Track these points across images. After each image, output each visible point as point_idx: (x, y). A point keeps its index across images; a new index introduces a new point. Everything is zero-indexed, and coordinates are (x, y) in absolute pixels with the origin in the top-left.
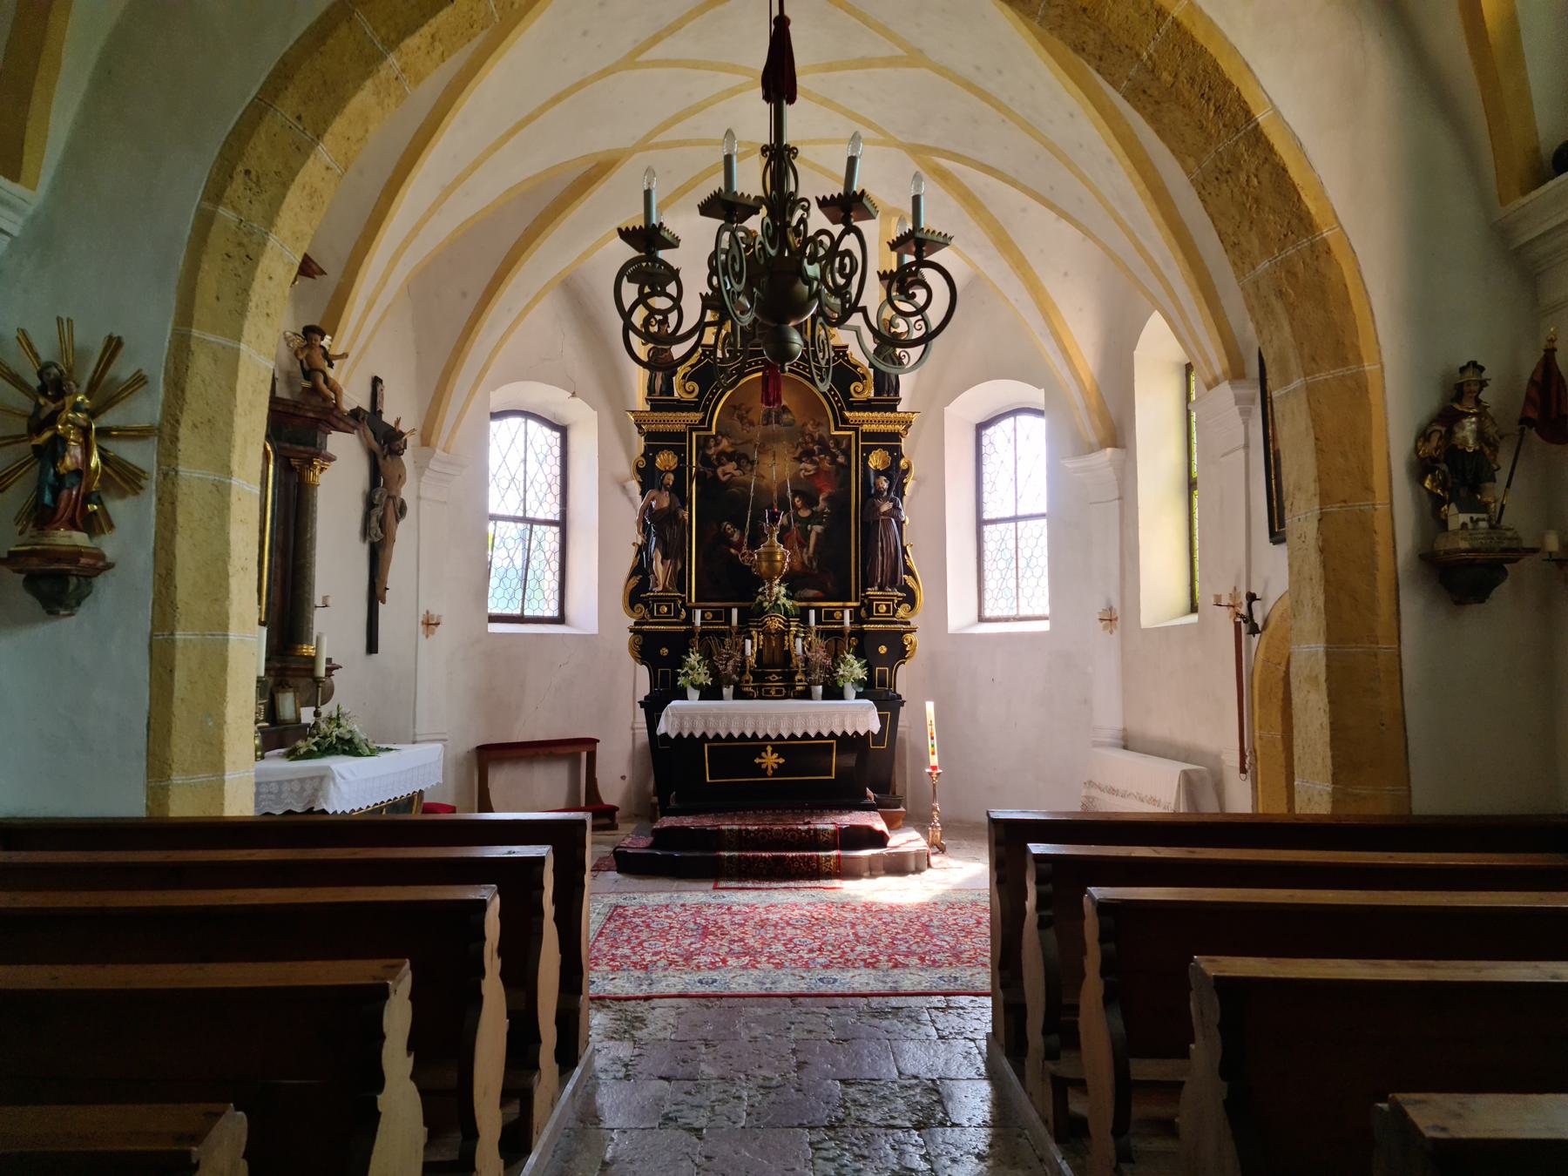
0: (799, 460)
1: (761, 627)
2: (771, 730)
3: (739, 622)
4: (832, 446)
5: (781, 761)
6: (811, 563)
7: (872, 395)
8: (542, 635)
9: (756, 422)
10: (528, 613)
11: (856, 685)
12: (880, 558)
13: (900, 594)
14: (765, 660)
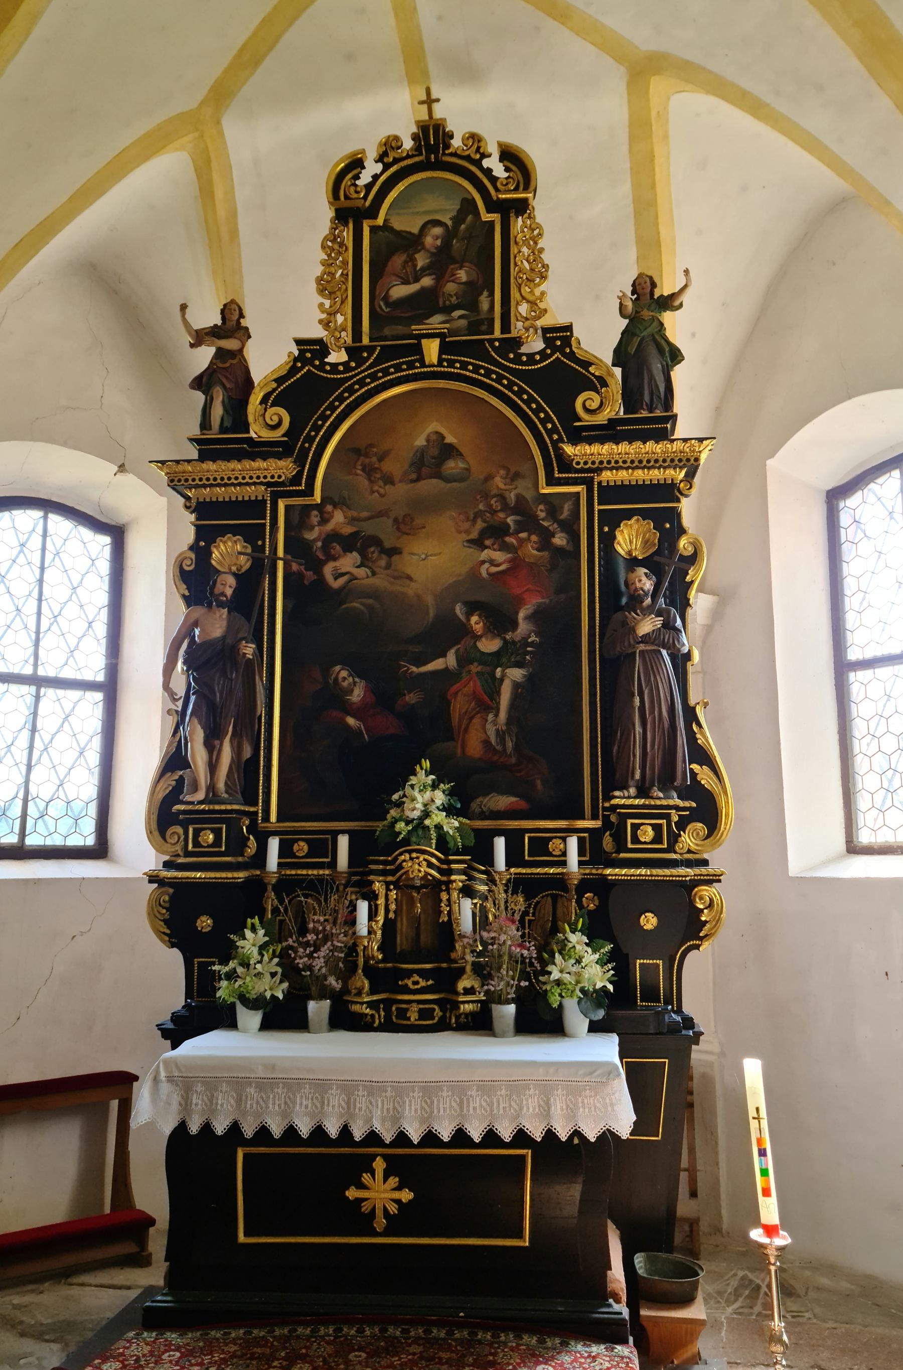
0: (479, 543)
1: (393, 873)
2: (383, 1120)
3: (352, 862)
4: (542, 515)
5: (406, 1196)
7: (622, 413)
8: (37, 882)
10: (31, 841)
11: (587, 1004)
12: (638, 729)
13: (681, 803)
14: (402, 941)
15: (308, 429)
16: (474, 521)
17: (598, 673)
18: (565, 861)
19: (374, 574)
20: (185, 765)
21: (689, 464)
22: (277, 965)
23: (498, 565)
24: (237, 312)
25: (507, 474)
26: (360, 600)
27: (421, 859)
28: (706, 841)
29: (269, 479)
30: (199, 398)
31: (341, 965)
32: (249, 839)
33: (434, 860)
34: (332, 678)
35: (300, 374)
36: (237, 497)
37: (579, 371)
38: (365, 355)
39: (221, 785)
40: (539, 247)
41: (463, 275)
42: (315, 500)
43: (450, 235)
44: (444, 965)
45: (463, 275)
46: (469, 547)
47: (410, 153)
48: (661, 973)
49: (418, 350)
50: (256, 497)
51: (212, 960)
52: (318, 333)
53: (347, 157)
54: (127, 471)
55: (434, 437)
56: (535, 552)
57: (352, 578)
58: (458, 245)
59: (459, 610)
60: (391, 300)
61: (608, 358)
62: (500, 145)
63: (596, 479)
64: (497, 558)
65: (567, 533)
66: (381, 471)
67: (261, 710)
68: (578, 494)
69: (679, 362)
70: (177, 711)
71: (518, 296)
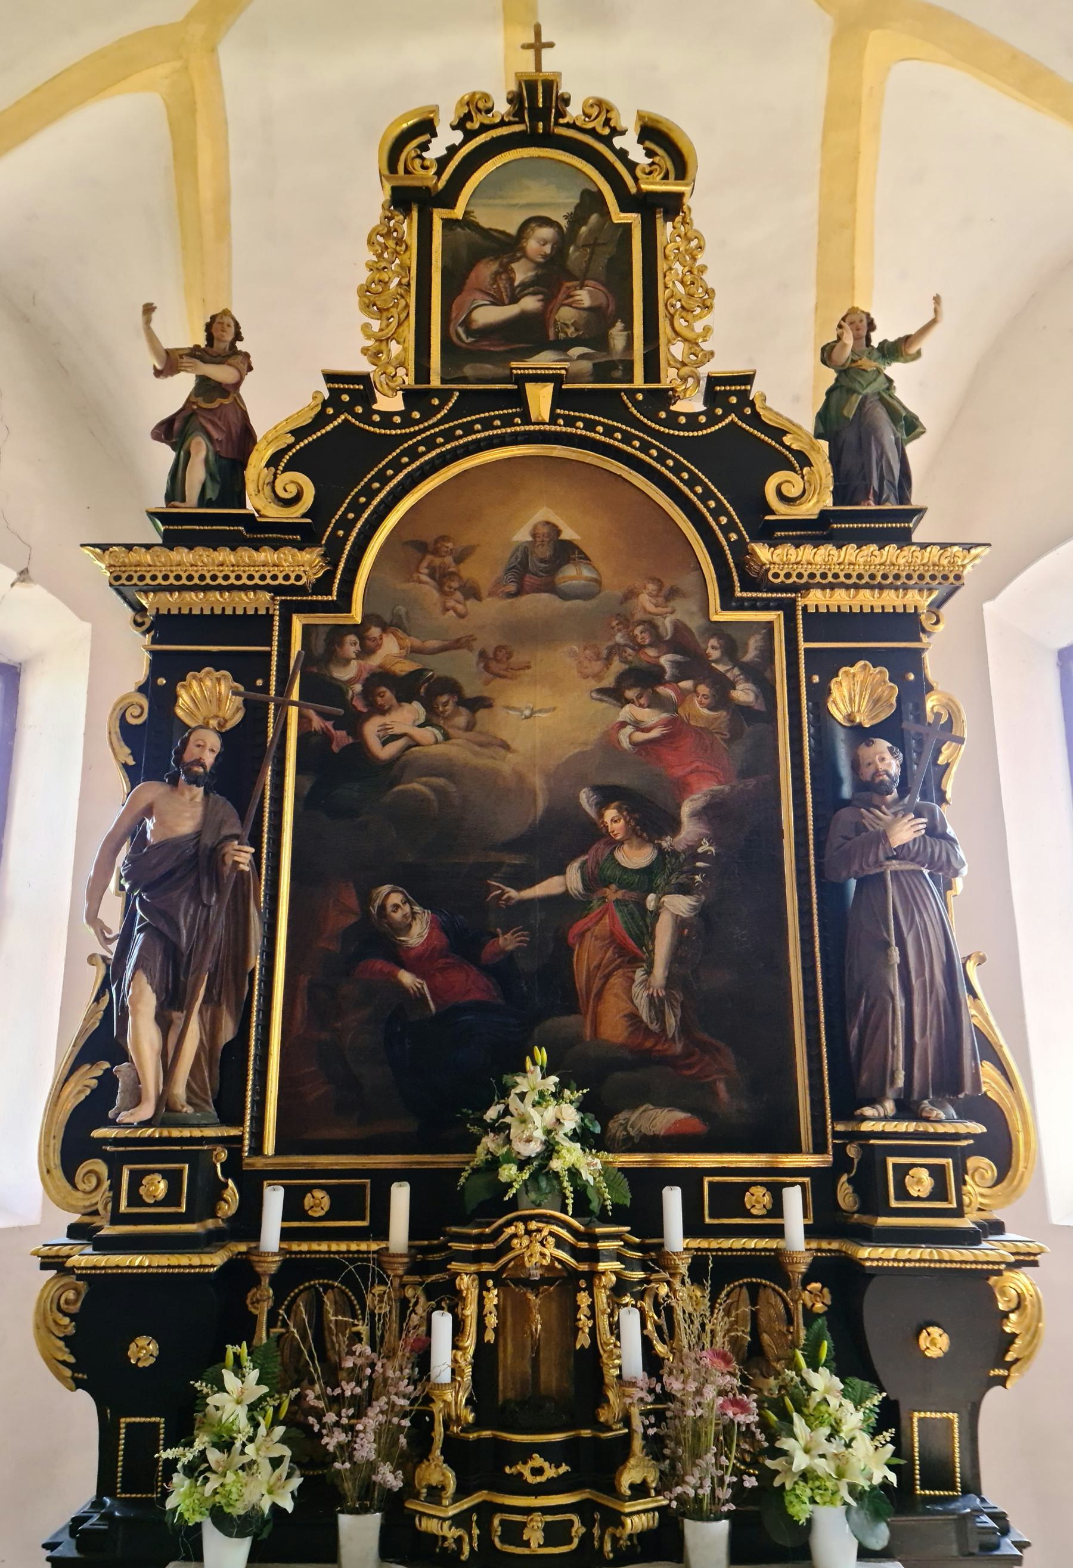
0: (615, 694)
1: (493, 1256)
3: (415, 1230)
4: (715, 654)
6: (660, 1016)
9: (485, 587)
14: (506, 1387)
15: (342, 509)
16: (608, 660)
17: (815, 906)
18: (782, 1226)
19: (447, 737)
20: (119, 1053)
21: (946, 584)
22: (283, 1440)
23: (648, 730)
24: (232, 330)
25: (660, 590)
26: (424, 779)
27: (545, 1233)
28: (995, 1189)
29: (280, 581)
30: (165, 455)
31: (403, 1440)
32: (226, 1185)
33: (564, 1233)
34: (376, 905)
35: (331, 426)
36: (223, 609)
37: (766, 443)
38: (436, 402)
39: (180, 1090)
40: (699, 263)
41: (584, 297)
42: (353, 617)
43: (564, 240)
44: (586, 1433)
45: (584, 297)
46: (601, 700)
47: (506, 119)
48: (956, 1435)
49: (519, 399)
50: (256, 609)
51: (153, 1419)
52: (362, 365)
53: (411, 114)
54: (31, 580)
55: (545, 530)
56: (705, 711)
57: (411, 743)
58: (577, 254)
59: (586, 799)
60: (475, 326)
61: (808, 424)
62: (640, 116)
63: (801, 603)
64: (645, 719)
65: (754, 683)
66: (461, 578)
67: (256, 962)
68: (770, 624)
69: (917, 436)
70: (104, 959)
71: (669, 330)
